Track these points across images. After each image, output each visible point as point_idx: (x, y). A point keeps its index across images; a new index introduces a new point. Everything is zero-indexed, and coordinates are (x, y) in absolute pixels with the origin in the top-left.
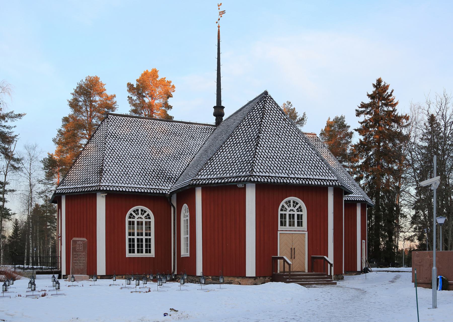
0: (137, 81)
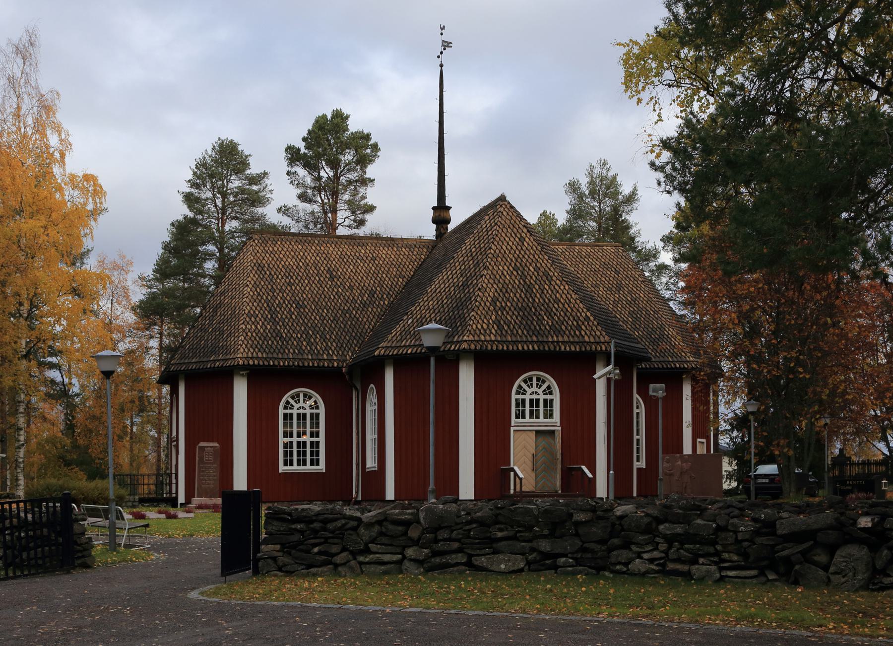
0: (304, 139)
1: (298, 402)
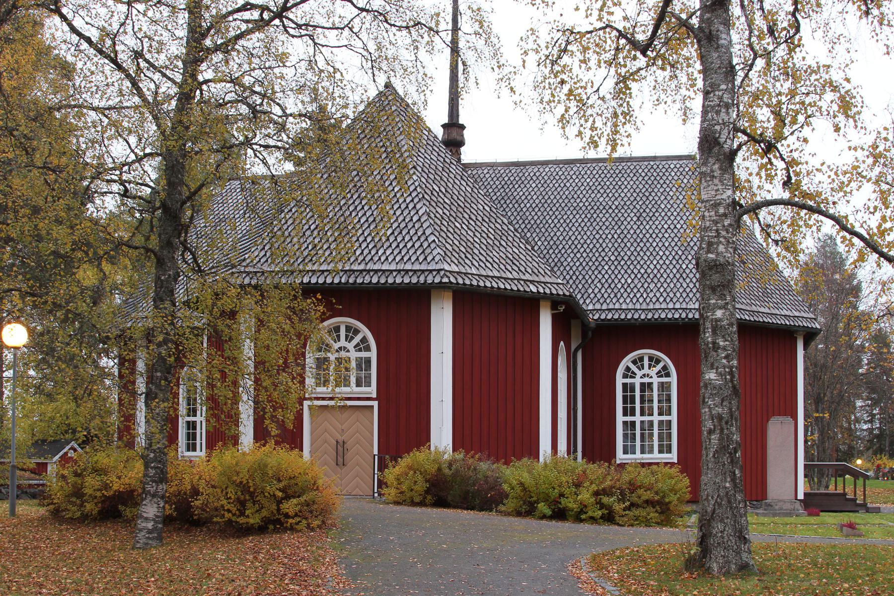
1: (641, 368)
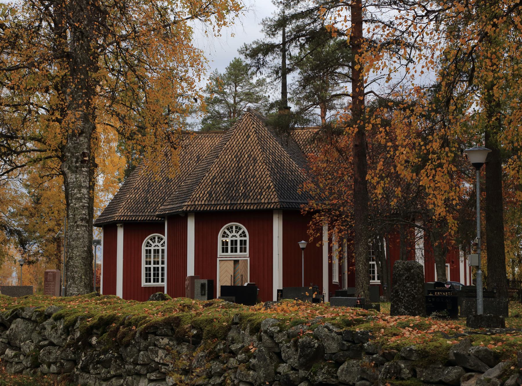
1: (154, 242)
